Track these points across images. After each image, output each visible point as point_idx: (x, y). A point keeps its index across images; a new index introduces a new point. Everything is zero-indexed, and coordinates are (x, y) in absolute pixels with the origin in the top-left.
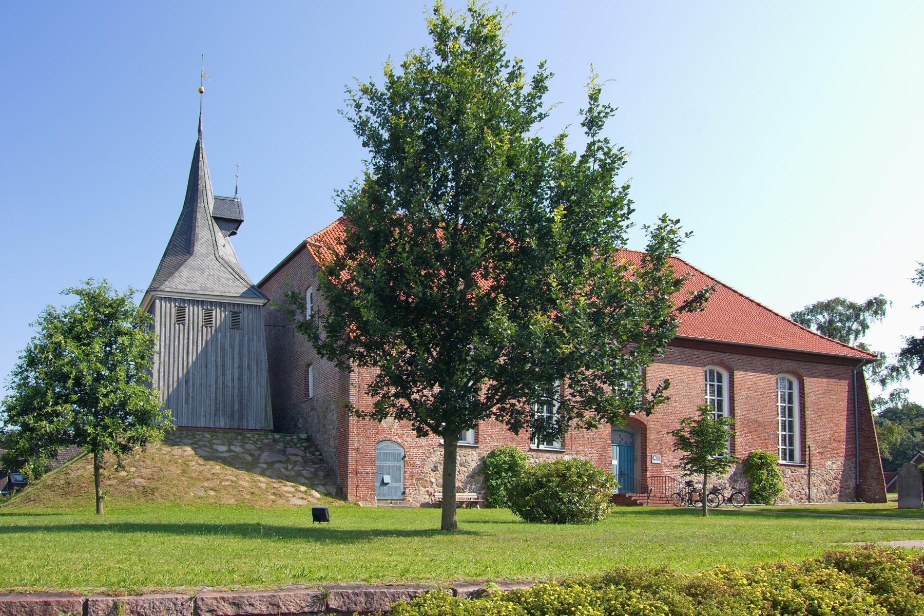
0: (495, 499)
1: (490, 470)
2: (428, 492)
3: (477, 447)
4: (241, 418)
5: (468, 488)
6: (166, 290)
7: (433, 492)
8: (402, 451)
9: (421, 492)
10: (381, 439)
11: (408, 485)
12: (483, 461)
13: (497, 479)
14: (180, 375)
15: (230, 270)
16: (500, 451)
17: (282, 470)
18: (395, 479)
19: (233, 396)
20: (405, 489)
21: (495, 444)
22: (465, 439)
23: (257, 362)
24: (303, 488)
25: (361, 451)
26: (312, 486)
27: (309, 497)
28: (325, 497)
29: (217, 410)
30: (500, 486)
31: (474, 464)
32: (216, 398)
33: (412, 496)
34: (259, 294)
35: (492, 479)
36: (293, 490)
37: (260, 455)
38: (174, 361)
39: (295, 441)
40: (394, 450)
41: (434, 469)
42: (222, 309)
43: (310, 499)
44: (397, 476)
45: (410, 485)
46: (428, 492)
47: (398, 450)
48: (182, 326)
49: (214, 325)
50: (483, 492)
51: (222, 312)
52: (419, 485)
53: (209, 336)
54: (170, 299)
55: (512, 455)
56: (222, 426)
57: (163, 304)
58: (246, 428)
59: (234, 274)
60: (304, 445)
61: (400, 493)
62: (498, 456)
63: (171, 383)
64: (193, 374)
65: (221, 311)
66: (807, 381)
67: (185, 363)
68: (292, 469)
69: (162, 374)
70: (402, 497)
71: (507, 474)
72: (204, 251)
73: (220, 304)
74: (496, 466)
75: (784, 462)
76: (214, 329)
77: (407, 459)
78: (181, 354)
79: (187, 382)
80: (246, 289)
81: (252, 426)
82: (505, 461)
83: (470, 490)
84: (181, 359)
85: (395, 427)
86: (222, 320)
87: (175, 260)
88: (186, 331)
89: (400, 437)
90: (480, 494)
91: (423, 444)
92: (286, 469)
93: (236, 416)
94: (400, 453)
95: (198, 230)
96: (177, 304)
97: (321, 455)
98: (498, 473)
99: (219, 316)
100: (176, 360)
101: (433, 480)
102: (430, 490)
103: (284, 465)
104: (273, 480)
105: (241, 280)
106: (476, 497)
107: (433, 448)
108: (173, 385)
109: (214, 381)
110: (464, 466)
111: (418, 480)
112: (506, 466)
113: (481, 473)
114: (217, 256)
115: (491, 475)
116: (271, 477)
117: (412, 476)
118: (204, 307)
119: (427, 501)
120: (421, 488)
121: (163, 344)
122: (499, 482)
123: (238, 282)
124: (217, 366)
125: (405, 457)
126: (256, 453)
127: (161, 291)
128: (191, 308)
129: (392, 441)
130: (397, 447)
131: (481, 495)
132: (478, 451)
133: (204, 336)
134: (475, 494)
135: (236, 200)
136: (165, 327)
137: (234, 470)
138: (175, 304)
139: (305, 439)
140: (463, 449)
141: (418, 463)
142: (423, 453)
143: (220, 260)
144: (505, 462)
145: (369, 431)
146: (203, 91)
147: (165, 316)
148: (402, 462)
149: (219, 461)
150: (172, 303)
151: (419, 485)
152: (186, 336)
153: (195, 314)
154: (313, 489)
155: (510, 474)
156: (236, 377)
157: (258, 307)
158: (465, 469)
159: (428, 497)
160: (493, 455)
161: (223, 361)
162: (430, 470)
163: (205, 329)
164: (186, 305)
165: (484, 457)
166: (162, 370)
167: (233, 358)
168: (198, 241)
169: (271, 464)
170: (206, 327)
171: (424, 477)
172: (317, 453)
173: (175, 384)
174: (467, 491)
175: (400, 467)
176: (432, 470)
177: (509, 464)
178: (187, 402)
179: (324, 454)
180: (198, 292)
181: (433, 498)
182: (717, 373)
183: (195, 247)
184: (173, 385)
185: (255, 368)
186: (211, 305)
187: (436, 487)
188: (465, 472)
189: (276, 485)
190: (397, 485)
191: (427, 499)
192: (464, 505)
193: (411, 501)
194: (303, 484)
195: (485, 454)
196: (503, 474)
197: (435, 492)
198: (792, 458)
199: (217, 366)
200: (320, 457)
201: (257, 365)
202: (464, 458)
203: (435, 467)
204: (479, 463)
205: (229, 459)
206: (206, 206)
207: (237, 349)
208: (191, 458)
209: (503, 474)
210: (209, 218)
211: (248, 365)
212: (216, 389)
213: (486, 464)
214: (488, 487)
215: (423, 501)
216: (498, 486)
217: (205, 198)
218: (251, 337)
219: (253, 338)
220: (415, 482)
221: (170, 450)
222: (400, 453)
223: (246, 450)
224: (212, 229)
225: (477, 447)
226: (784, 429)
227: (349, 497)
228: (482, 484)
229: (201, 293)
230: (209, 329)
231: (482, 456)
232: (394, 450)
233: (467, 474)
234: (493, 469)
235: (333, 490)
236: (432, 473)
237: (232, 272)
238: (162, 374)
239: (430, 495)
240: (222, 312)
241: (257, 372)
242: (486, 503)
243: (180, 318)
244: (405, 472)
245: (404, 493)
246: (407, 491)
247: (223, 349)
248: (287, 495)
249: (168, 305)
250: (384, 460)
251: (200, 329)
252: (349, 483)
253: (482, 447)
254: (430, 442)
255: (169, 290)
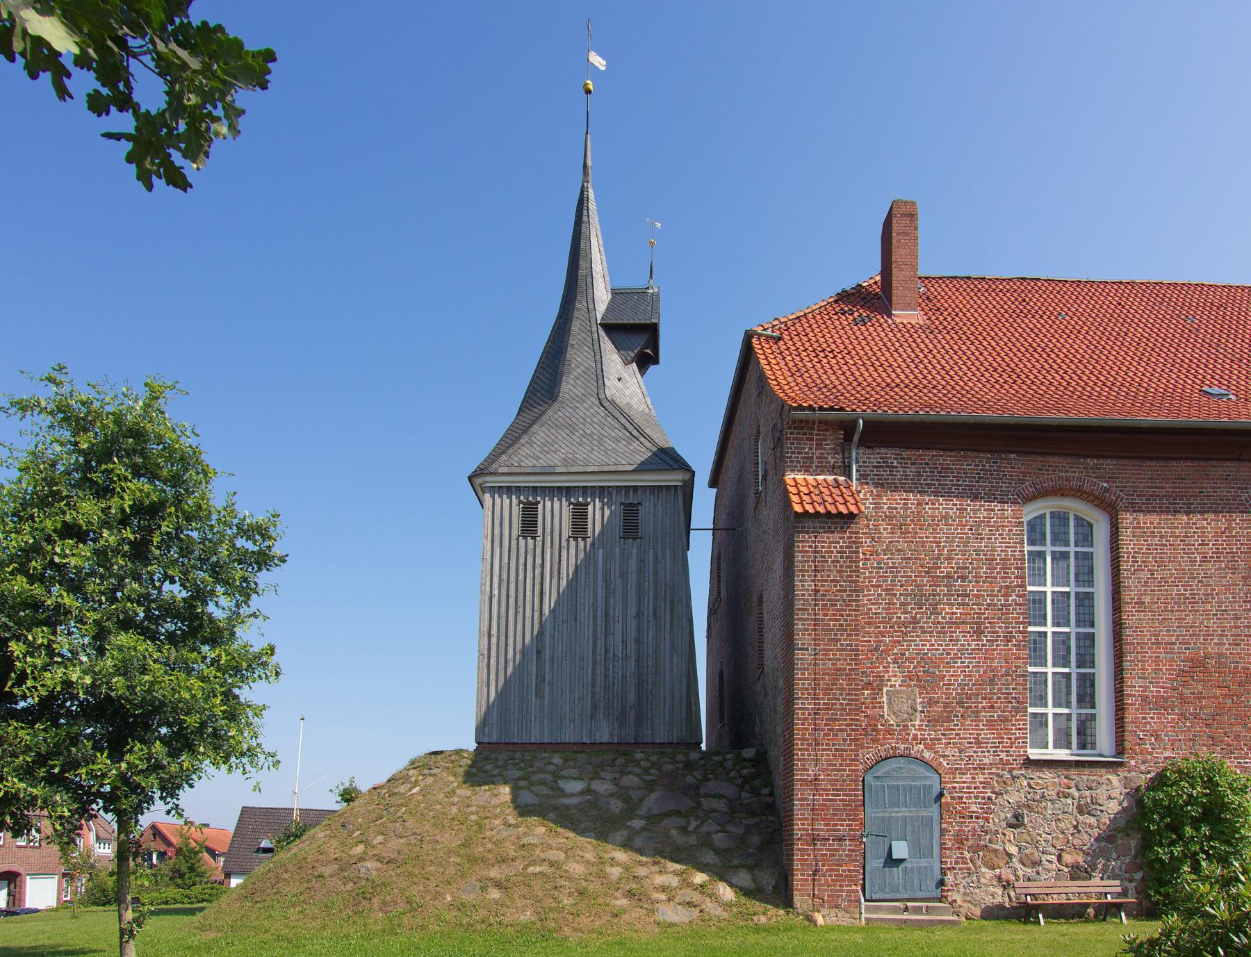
0: (1167, 896)
1: (1154, 821)
2: (999, 878)
3: (1121, 764)
4: (639, 722)
5: (1100, 866)
6: (500, 471)
7: (1012, 878)
8: (934, 781)
9: (982, 880)
10: (883, 754)
11: (950, 862)
12: (1136, 796)
13: (1172, 843)
14: (528, 639)
15: (623, 421)
16: (1180, 772)
17: (674, 832)
18: (918, 850)
19: (624, 676)
20: (945, 874)
21: (1167, 754)
22: (1093, 746)
23: (672, 603)
24: (700, 878)
25: (824, 784)
26: (721, 874)
27: (708, 900)
28: (743, 900)
29: (595, 707)
30: (1180, 861)
31: (1113, 807)
32: (594, 680)
33: (962, 890)
34: (671, 462)
35: (1161, 845)
36: (674, 881)
37: (642, 799)
38: (516, 614)
39: (729, 764)
40: (915, 778)
41: (1013, 821)
42: (606, 500)
43: (708, 905)
44: (924, 842)
45: (957, 863)
46: (999, 878)
47: (926, 778)
48: (581, 543)
49: (590, 533)
50: (1138, 876)
51: (606, 508)
52: (979, 863)
53: (582, 555)
54: (509, 490)
55: (1210, 779)
56: (605, 740)
57: (498, 500)
58: (649, 740)
59: (631, 428)
60: (744, 772)
61: (931, 884)
62: (1174, 784)
63: (510, 655)
64: (553, 637)
65: (603, 504)
66: (1126, 519)
67: (536, 615)
68: (696, 831)
69: (494, 640)
70: (938, 893)
71: (1198, 829)
72: (579, 391)
73: (602, 491)
74: (1169, 810)
75: (1063, 754)
76: (589, 541)
77: (947, 799)
78: (529, 599)
79: (539, 652)
80: (650, 454)
81: (661, 737)
82: (1191, 796)
83: (1104, 871)
84: (528, 607)
85: (917, 723)
86: (606, 519)
87: (529, 416)
88: (539, 551)
89: (928, 747)
90: (1131, 881)
91: (986, 761)
92: (684, 830)
93: (632, 717)
94: (931, 786)
95: (571, 353)
96: (522, 498)
97: (771, 794)
98: (1176, 828)
99: (598, 515)
100: (521, 610)
101: (1013, 850)
102: (1006, 873)
103: (680, 821)
104: (644, 859)
105: (642, 439)
106: (1119, 889)
107: (1010, 771)
108: (514, 661)
109: (591, 650)
110: (1089, 813)
111: (975, 849)
112: (1194, 811)
113: (1133, 829)
114: (602, 397)
115: (1158, 832)
116: (640, 851)
117: (960, 841)
118: (522, 498)
119: (998, 900)
120: (983, 870)
121: (496, 580)
122: (1177, 850)
123: (635, 444)
124: (595, 618)
125: (941, 795)
126: (635, 795)
127: (491, 474)
128: (548, 504)
129: (909, 756)
130: (922, 771)
131: (1133, 884)
132: (1122, 773)
133: (572, 555)
134: (1117, 882)
135: (651, 291)
136: (552, 547)
137: (572, 835)
138: (518, 498)
139: (750, 760)
140: (1086, 771)
141: (974, 808)
142: (986, 784)
143: (607, 404)
144: (1191, 800)
145: (841, 736)
146: (591, 87)
147: (501, 525)
148: (936, 807)
149: (552, 815)
150: (514, 497)
151: (979, 863)
152: (539, 561)
153: (553, 512)
154: (722, 879)
155: (1205, 829)
156: (632, 635)
157: (673, 490)
158: (1092, 820)
159: (999, 891)
160: (1160, 781)
161: (607, 606)
162: (1004, 824)
163: (573, 543)
164: (539, 499)
165: (1138, 789)
166: (494, 631)
167: (625, 598)
168: (569, 373)
169: (653, 819)
170: (576, 539)
171: (990, 841)
172: (765, 791)
173: (518, 657)
174: (1097, 875)
175: (931, 819)
176: (1010, 826)
177: (1203, 805)
178: (539, 693)
179: (777, 792)
180: (558, 470)
181: (1012, 894)
182: (1078, 519)
183: (563, 385)
184: (514, 661)
185: (668, 615)
186: (585, 495)
187: (1019, 866)
188: (1091, 826)
189: (642, 871)
190: (924, 863)
191: (998, 897)
192: (1091, 911)
193: (959, 902)
194: (702, 868)
195: (1142, 780)
196: (1188, 831)
197: (1017, 878)
198: (1085, 742)
199: (595, 618)
200: (769, 800)
201: (672, 609)
202: (1088, 793)
203: (1016, 816)
204: (1125, 804)
205: (573, 811)
206: (591, 306)
207: (633, 579)
208: (498, 810)
209: (1188, 831)
210: (594, 329)
211: (655, 611)
212: (595, 662)
213: (1144, 807)
214: (1150, 864)
215: (989, 901)
216: (1176, 862)
217: (590, 291)
218: (660, 554)
219: (664, 555)
220: (967, 855)
221: (469, 793)
222: (931, 786)
223: (621, 788)
224: (597, 347)
225: (1121, 764)
226: (1061, 660)
227: (797, 899)
228: (1135, 857)
229: (564, 470)
230: (581, 543)
231: (1134, 786)
232: (915, 778)
233: (1096, 832)
234: (1162, 818)
235: (768, 880)
236: (1009, 832)
237: (627, 424)
238: (494, 640)
239: (1004, 887)
240: (606, 508)
241: (672, 623)
242: (1145, 904)
243: (529, 525)
244: (943, 832)
245: (941, 883)
246: (949, 879)
247: (607, 582)
248: (656, 895)
249: (507, 501)
250: (892, 805)
251: (564, 543)
252: (797, 865)
253: (1133, 763)
254: (1003, 755)
255: (505, 470)
